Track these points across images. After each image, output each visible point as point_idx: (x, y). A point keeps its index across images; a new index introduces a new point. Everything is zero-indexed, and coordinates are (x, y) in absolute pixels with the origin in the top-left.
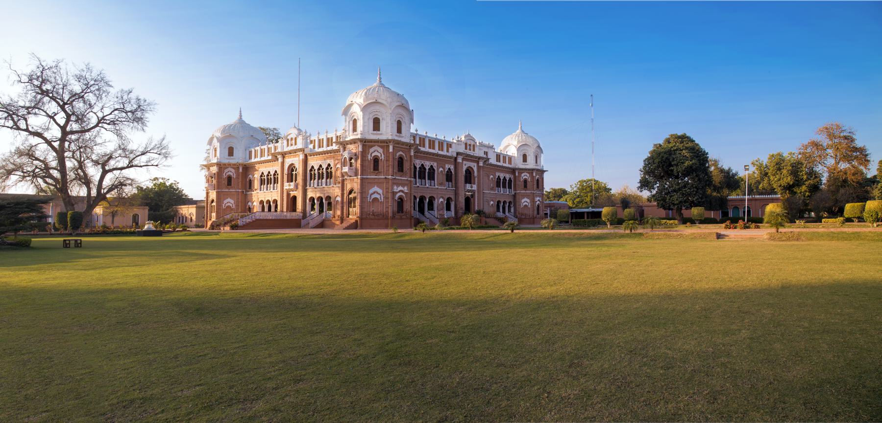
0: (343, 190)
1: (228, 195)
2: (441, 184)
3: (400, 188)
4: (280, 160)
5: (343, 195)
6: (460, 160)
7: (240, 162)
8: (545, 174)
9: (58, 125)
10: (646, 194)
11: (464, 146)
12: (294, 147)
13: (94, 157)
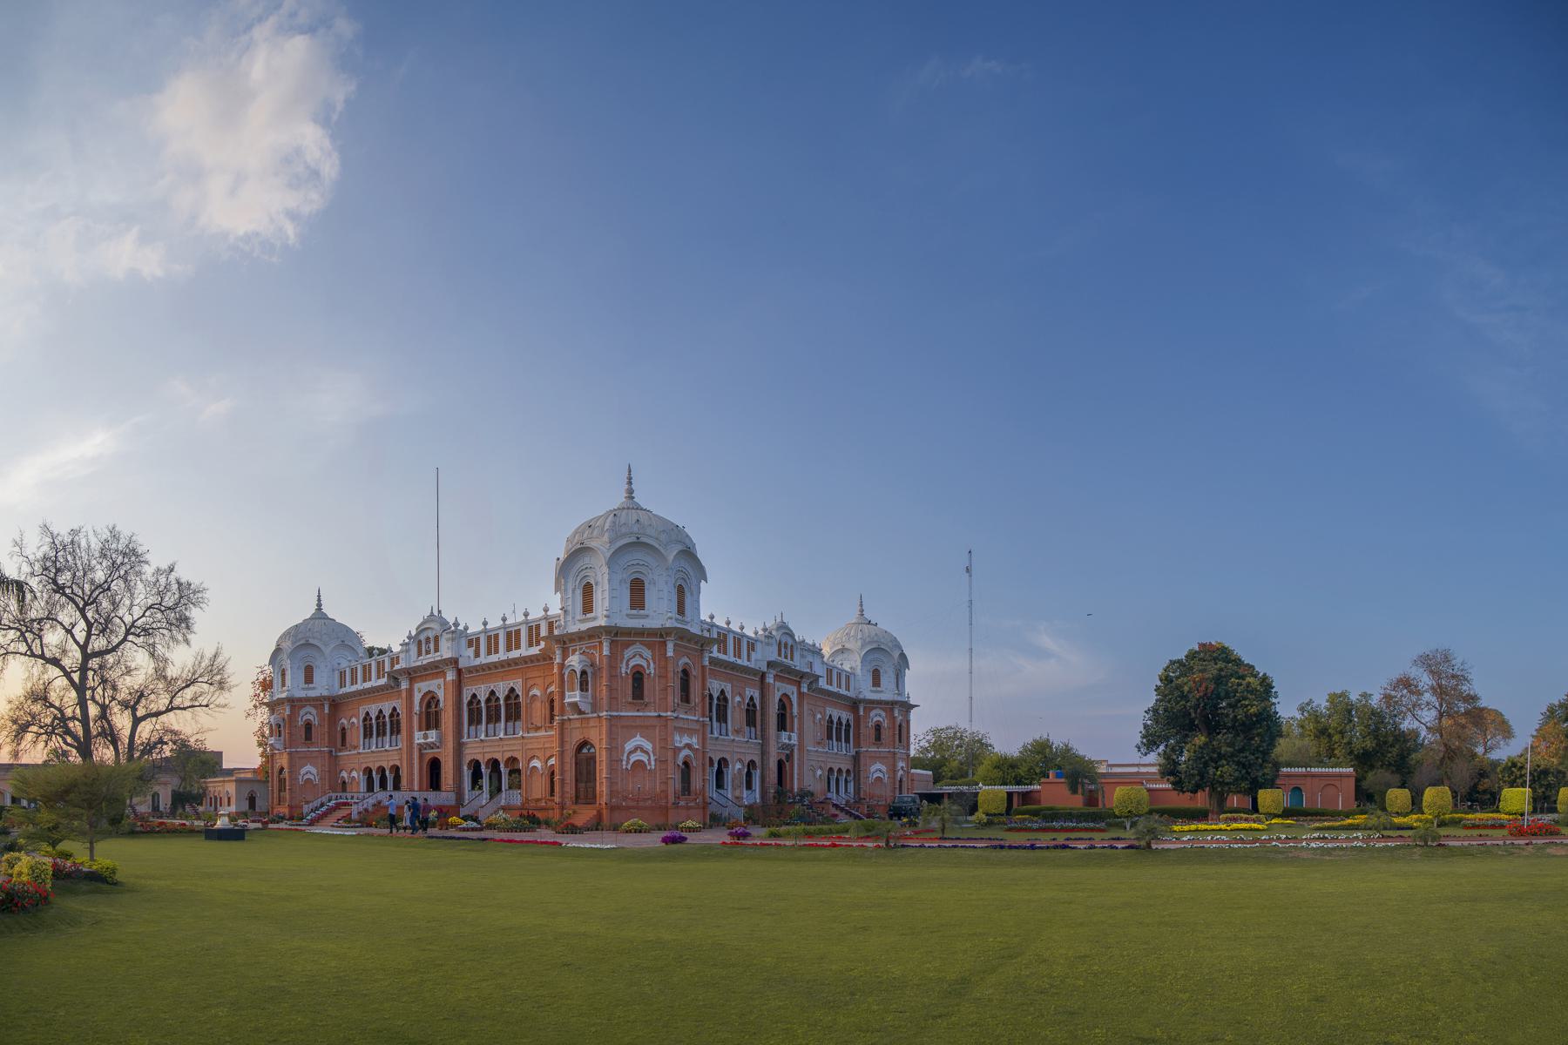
0: (562, 743)
1: (307, 758)
2: (737, 732)
3: (686, 740)
4: (404, 685)
5: (562, 753)
6: (770, 679)
7: (325, 693)
8: (913, 714)
9: (77, 643)
10: (1153, 757)
11: (776, 648)
12: (432, 657)
13: (120, 696)
